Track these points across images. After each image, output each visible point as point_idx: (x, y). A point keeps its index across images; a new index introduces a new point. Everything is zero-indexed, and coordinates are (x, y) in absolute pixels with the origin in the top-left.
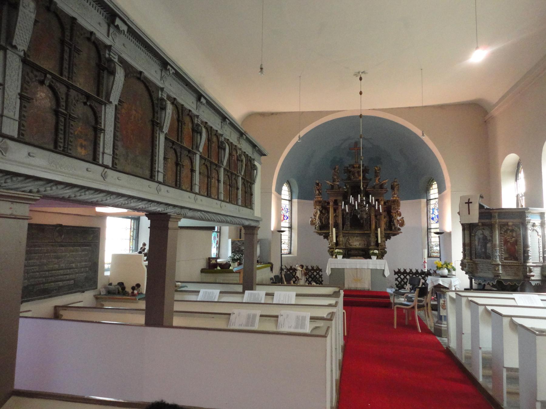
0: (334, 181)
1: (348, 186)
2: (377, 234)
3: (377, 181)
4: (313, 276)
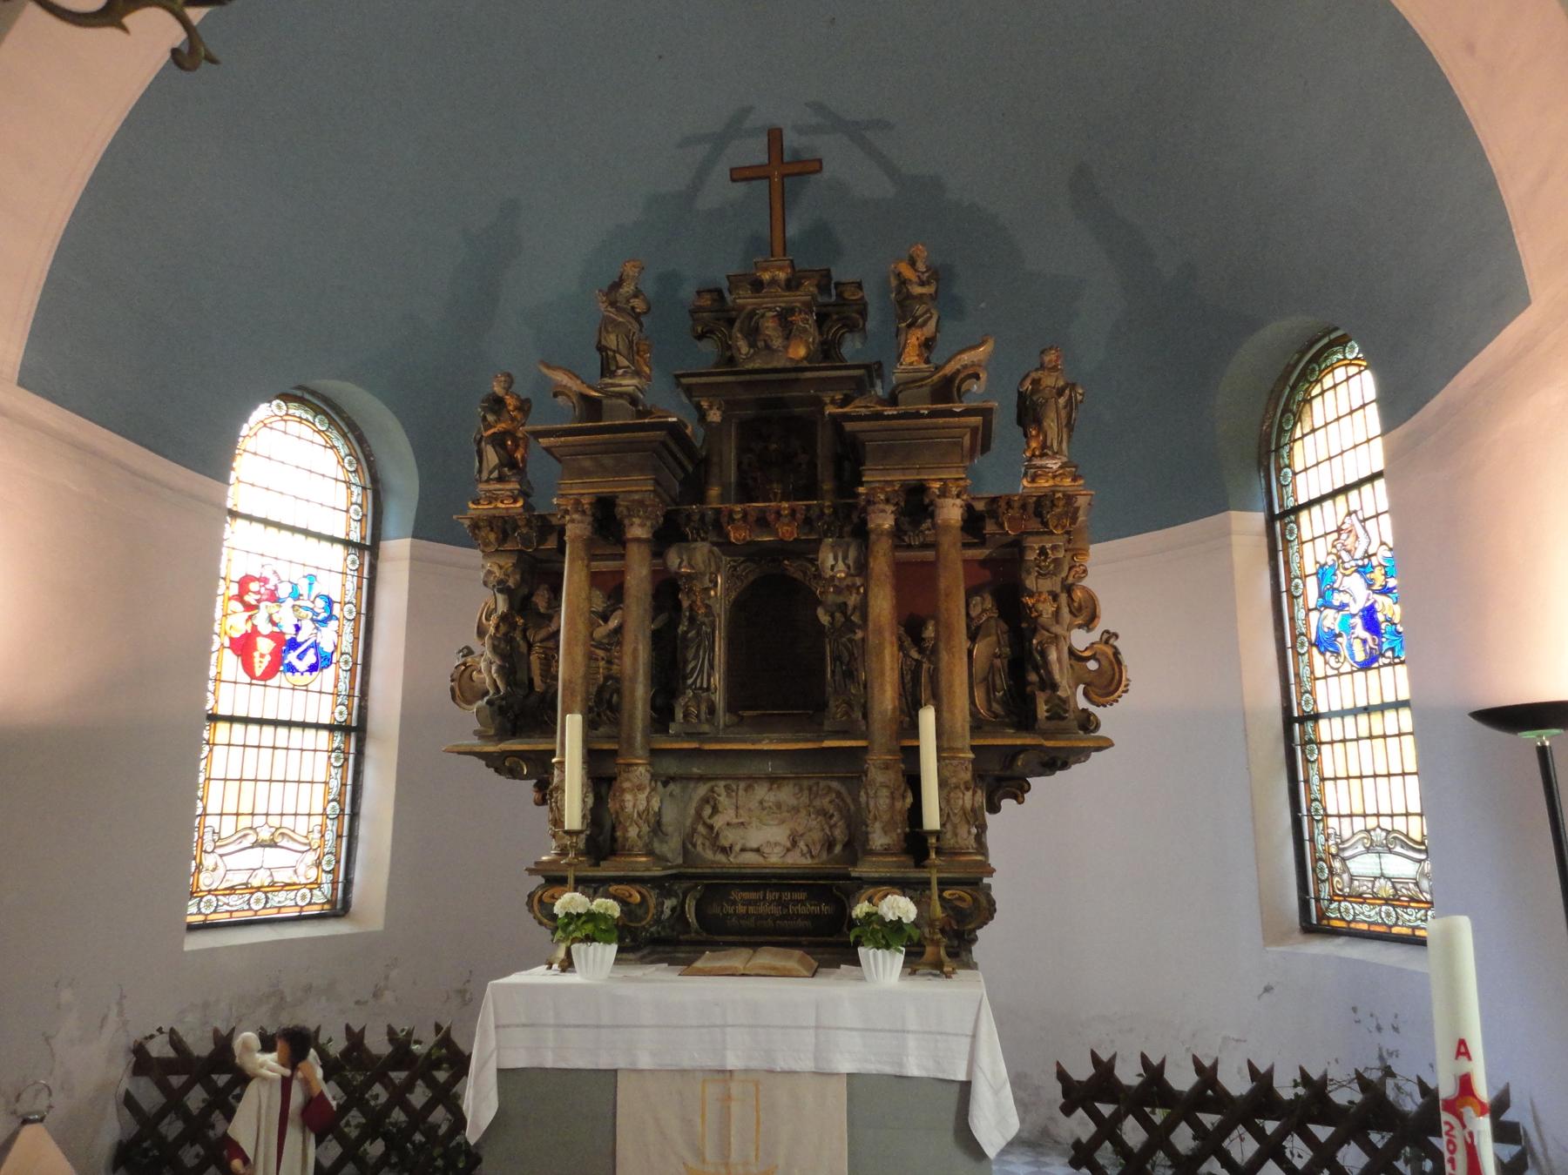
0: (607, 369)
1: (715, 416)
2: (913, 754)
3: (911, 357)
4: (398, 1115)
